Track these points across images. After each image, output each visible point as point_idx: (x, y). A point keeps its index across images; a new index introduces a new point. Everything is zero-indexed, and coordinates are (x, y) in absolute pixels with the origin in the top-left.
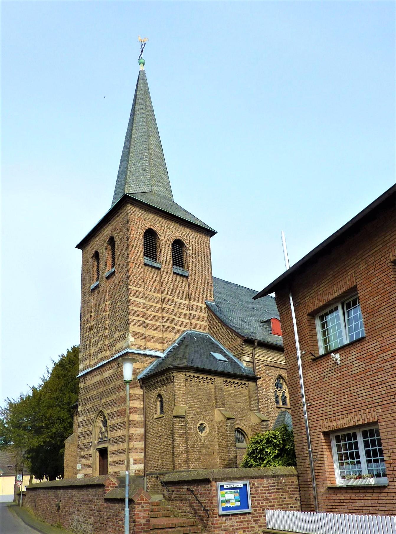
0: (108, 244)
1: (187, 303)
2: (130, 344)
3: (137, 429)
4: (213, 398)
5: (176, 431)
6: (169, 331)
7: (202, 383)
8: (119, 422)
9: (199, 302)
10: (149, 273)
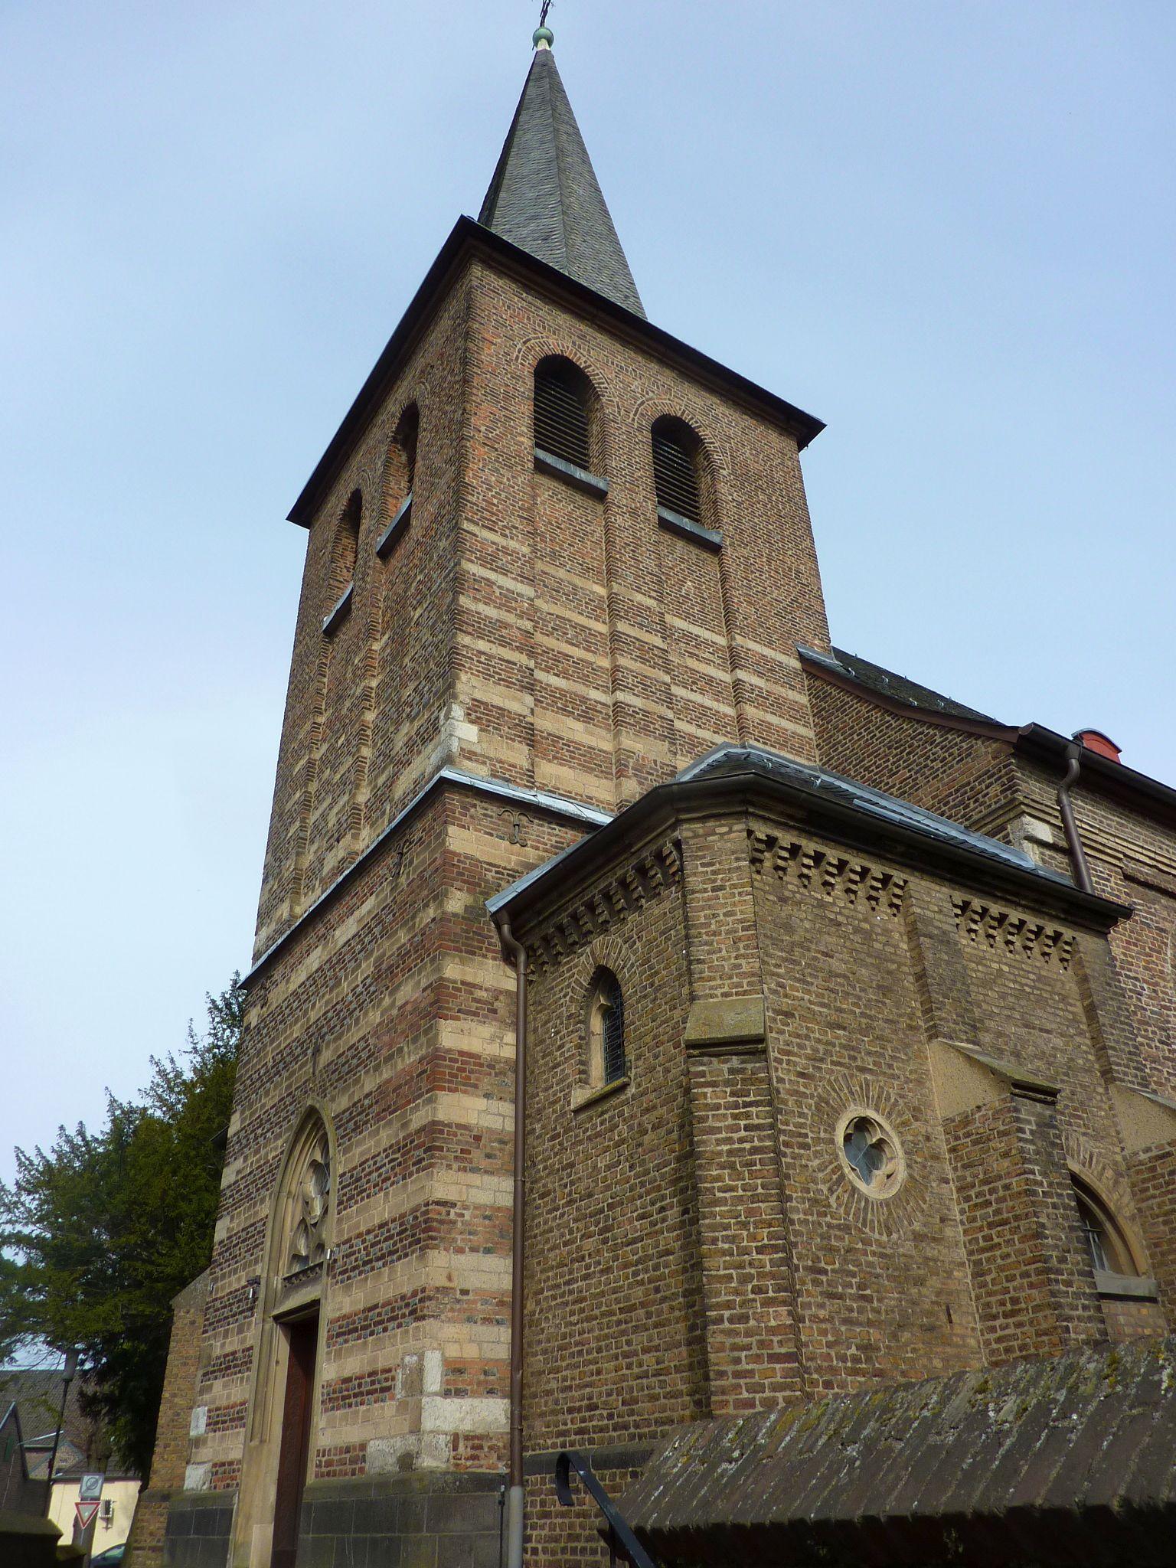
0: (395, 440)
1: (722, 641)
2: (455, 747)
3: (475, 1179)
4: (909, 982)
5: (710, 1144)
6: (645, 730)
7: (838, 891)
8: (385, 1144)
9: (770, 644)
10: (554, 503)
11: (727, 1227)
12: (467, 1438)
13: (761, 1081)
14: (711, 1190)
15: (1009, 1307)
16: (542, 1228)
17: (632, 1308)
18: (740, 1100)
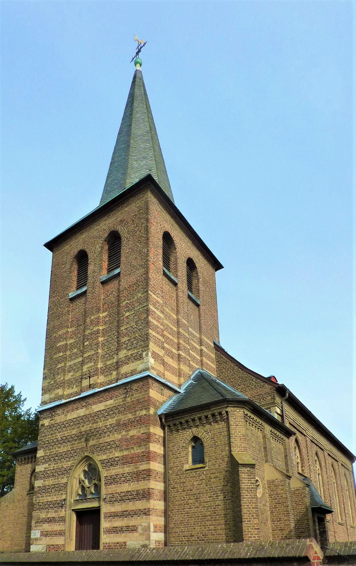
0: (105, 240)
3: (157, 483)
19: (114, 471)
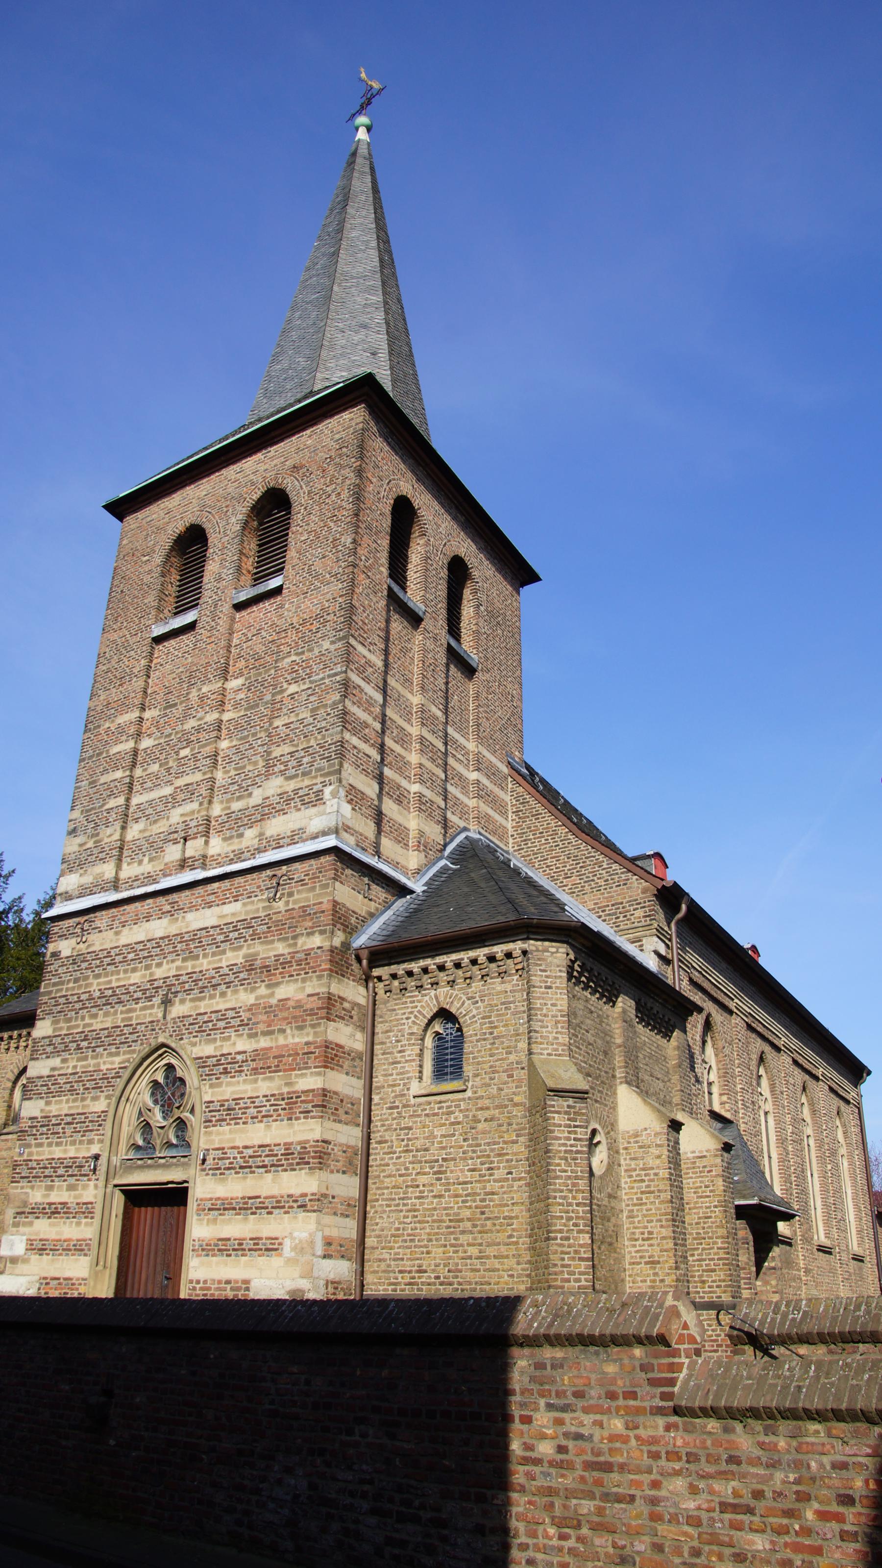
11: (562, 1191)
12: (333, 1283)
13: (583, 1114)
14: (555, 1170)
15: (646, 1235)
16: (378, 1162)
17: (462, 1220)
18: (572, 1123)
19: (231, 1089)
